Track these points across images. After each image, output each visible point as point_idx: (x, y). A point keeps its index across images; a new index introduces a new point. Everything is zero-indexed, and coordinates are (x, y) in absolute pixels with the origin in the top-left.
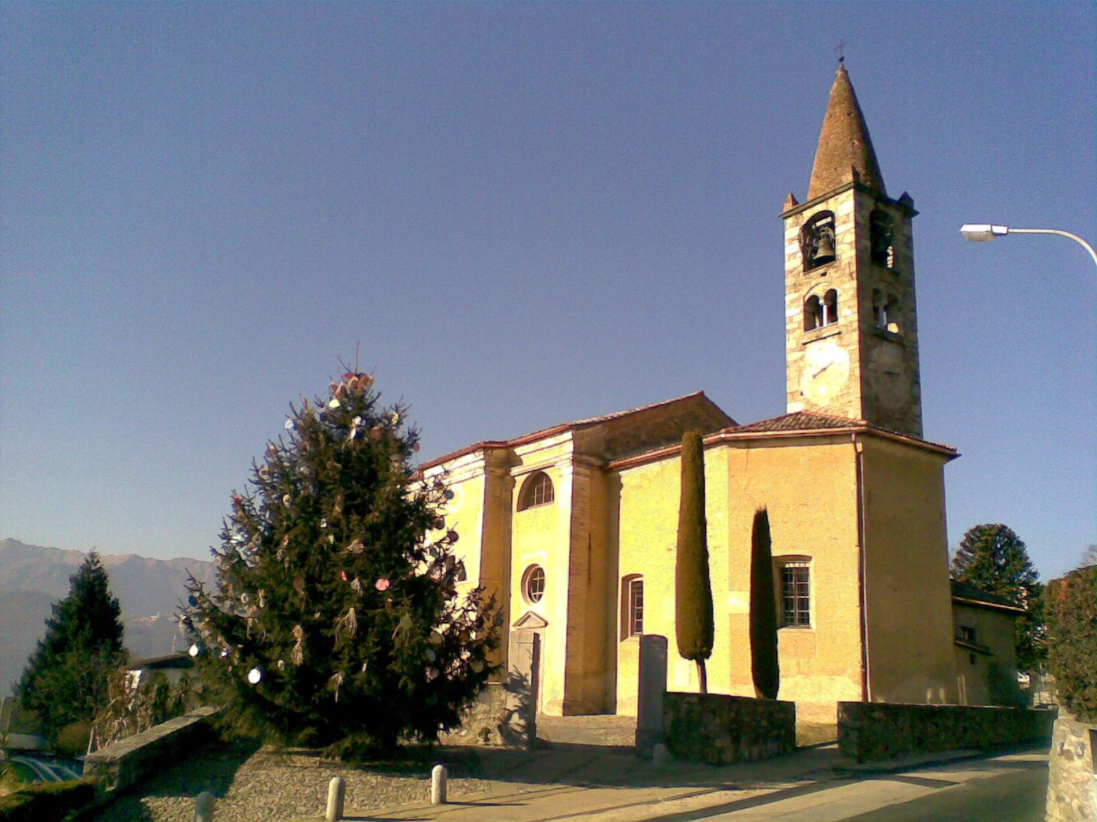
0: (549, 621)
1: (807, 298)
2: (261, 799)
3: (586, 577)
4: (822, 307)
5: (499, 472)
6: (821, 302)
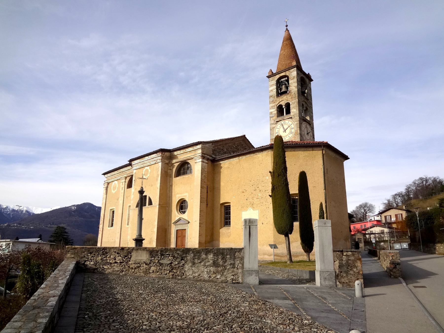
0: (190, 221)
1: (278, 105)
2: (239, 316)
3: (206, 204)
4: (284, 109)
5: (167, 161)
6: (284, 107)
